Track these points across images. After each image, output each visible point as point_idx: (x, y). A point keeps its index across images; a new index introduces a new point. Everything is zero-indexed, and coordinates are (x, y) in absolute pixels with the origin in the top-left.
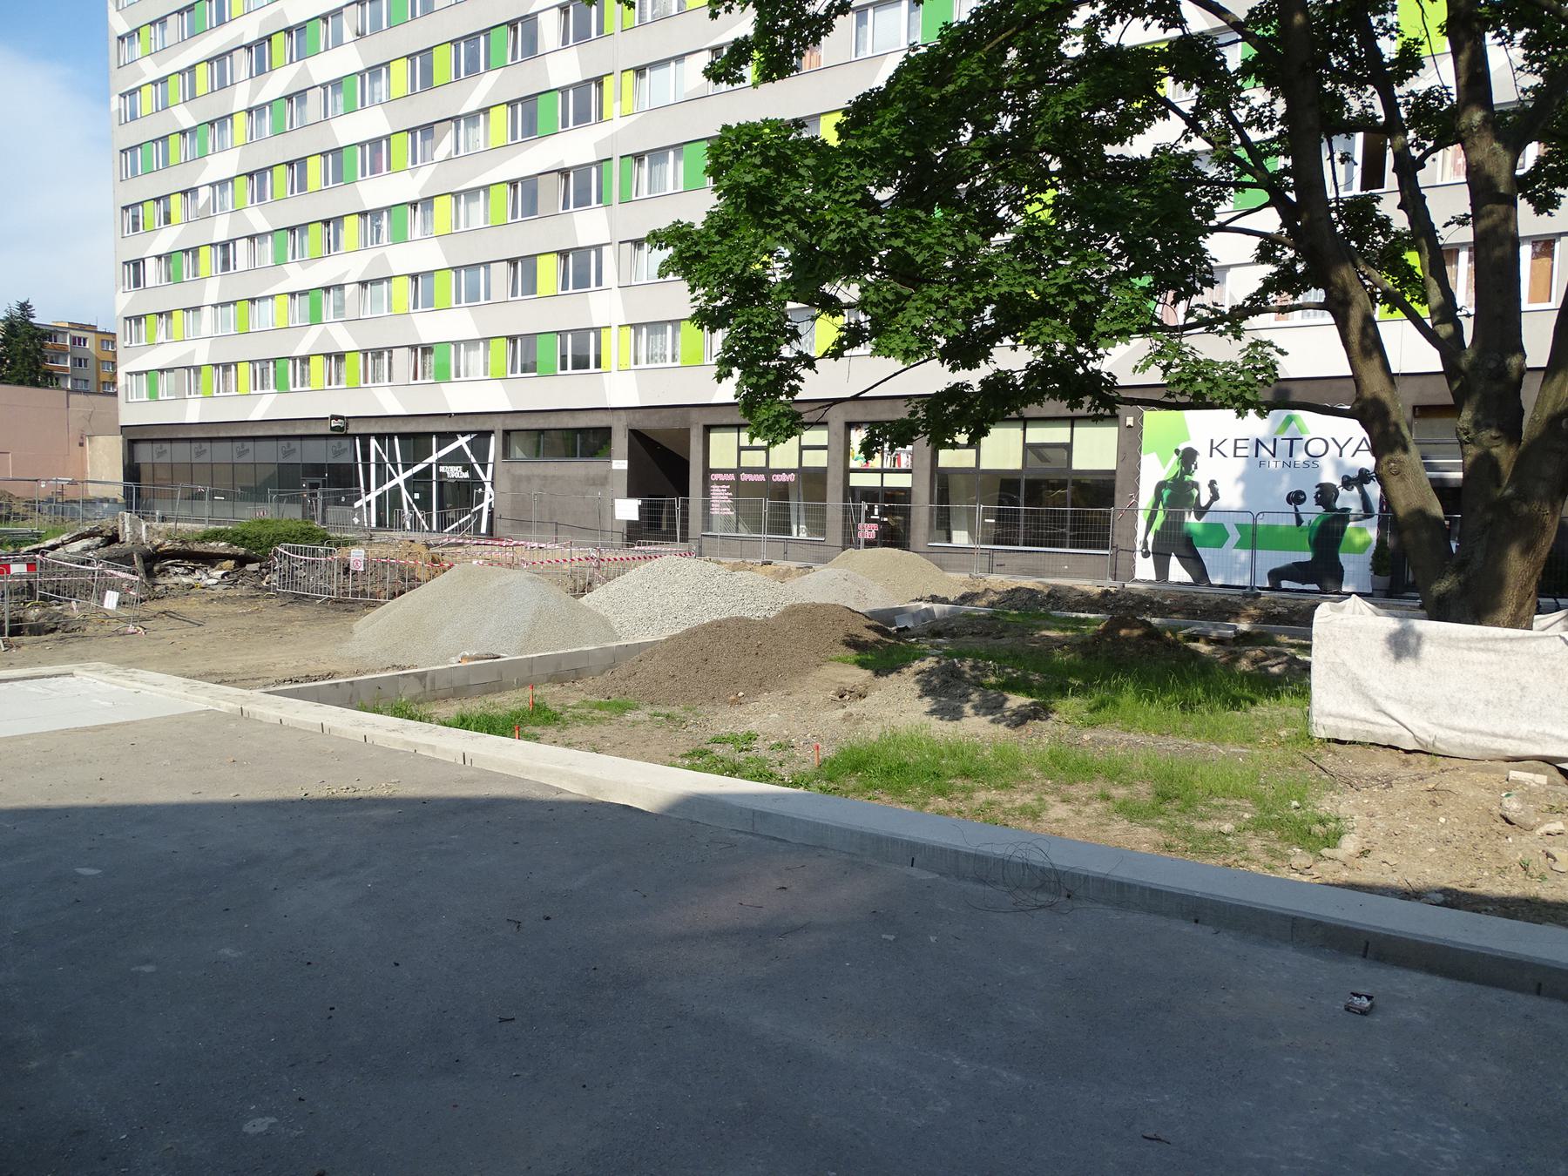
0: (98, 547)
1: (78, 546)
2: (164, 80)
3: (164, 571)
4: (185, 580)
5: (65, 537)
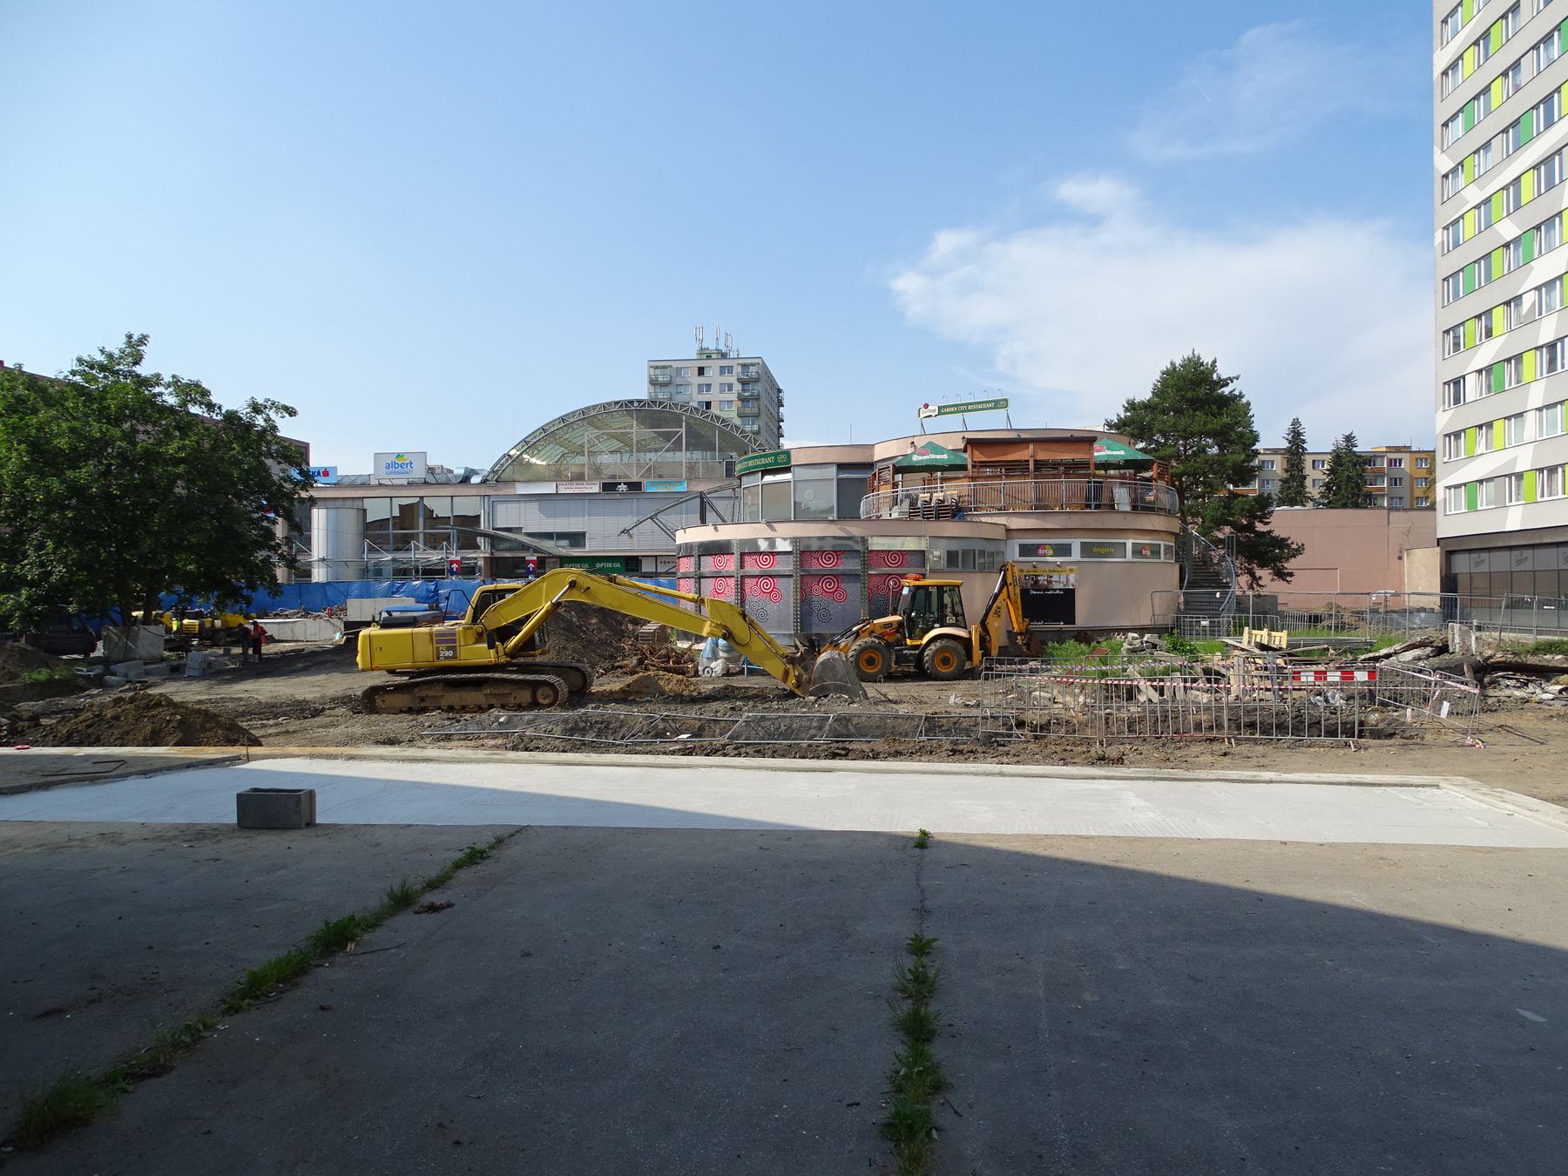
0: (1428, 657)
1: (1409, 656)
2: (1487, 201)
3: (1494, 683)
4: (1518, 693)
5: (1397, 647)
